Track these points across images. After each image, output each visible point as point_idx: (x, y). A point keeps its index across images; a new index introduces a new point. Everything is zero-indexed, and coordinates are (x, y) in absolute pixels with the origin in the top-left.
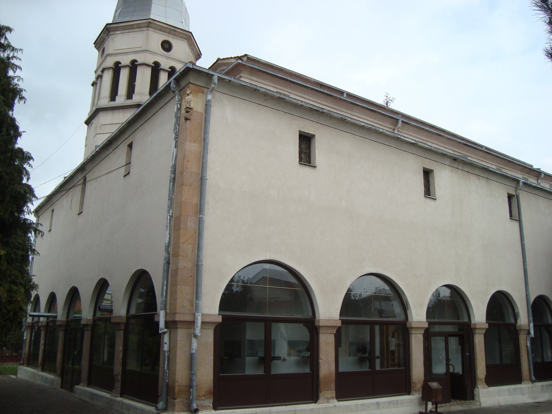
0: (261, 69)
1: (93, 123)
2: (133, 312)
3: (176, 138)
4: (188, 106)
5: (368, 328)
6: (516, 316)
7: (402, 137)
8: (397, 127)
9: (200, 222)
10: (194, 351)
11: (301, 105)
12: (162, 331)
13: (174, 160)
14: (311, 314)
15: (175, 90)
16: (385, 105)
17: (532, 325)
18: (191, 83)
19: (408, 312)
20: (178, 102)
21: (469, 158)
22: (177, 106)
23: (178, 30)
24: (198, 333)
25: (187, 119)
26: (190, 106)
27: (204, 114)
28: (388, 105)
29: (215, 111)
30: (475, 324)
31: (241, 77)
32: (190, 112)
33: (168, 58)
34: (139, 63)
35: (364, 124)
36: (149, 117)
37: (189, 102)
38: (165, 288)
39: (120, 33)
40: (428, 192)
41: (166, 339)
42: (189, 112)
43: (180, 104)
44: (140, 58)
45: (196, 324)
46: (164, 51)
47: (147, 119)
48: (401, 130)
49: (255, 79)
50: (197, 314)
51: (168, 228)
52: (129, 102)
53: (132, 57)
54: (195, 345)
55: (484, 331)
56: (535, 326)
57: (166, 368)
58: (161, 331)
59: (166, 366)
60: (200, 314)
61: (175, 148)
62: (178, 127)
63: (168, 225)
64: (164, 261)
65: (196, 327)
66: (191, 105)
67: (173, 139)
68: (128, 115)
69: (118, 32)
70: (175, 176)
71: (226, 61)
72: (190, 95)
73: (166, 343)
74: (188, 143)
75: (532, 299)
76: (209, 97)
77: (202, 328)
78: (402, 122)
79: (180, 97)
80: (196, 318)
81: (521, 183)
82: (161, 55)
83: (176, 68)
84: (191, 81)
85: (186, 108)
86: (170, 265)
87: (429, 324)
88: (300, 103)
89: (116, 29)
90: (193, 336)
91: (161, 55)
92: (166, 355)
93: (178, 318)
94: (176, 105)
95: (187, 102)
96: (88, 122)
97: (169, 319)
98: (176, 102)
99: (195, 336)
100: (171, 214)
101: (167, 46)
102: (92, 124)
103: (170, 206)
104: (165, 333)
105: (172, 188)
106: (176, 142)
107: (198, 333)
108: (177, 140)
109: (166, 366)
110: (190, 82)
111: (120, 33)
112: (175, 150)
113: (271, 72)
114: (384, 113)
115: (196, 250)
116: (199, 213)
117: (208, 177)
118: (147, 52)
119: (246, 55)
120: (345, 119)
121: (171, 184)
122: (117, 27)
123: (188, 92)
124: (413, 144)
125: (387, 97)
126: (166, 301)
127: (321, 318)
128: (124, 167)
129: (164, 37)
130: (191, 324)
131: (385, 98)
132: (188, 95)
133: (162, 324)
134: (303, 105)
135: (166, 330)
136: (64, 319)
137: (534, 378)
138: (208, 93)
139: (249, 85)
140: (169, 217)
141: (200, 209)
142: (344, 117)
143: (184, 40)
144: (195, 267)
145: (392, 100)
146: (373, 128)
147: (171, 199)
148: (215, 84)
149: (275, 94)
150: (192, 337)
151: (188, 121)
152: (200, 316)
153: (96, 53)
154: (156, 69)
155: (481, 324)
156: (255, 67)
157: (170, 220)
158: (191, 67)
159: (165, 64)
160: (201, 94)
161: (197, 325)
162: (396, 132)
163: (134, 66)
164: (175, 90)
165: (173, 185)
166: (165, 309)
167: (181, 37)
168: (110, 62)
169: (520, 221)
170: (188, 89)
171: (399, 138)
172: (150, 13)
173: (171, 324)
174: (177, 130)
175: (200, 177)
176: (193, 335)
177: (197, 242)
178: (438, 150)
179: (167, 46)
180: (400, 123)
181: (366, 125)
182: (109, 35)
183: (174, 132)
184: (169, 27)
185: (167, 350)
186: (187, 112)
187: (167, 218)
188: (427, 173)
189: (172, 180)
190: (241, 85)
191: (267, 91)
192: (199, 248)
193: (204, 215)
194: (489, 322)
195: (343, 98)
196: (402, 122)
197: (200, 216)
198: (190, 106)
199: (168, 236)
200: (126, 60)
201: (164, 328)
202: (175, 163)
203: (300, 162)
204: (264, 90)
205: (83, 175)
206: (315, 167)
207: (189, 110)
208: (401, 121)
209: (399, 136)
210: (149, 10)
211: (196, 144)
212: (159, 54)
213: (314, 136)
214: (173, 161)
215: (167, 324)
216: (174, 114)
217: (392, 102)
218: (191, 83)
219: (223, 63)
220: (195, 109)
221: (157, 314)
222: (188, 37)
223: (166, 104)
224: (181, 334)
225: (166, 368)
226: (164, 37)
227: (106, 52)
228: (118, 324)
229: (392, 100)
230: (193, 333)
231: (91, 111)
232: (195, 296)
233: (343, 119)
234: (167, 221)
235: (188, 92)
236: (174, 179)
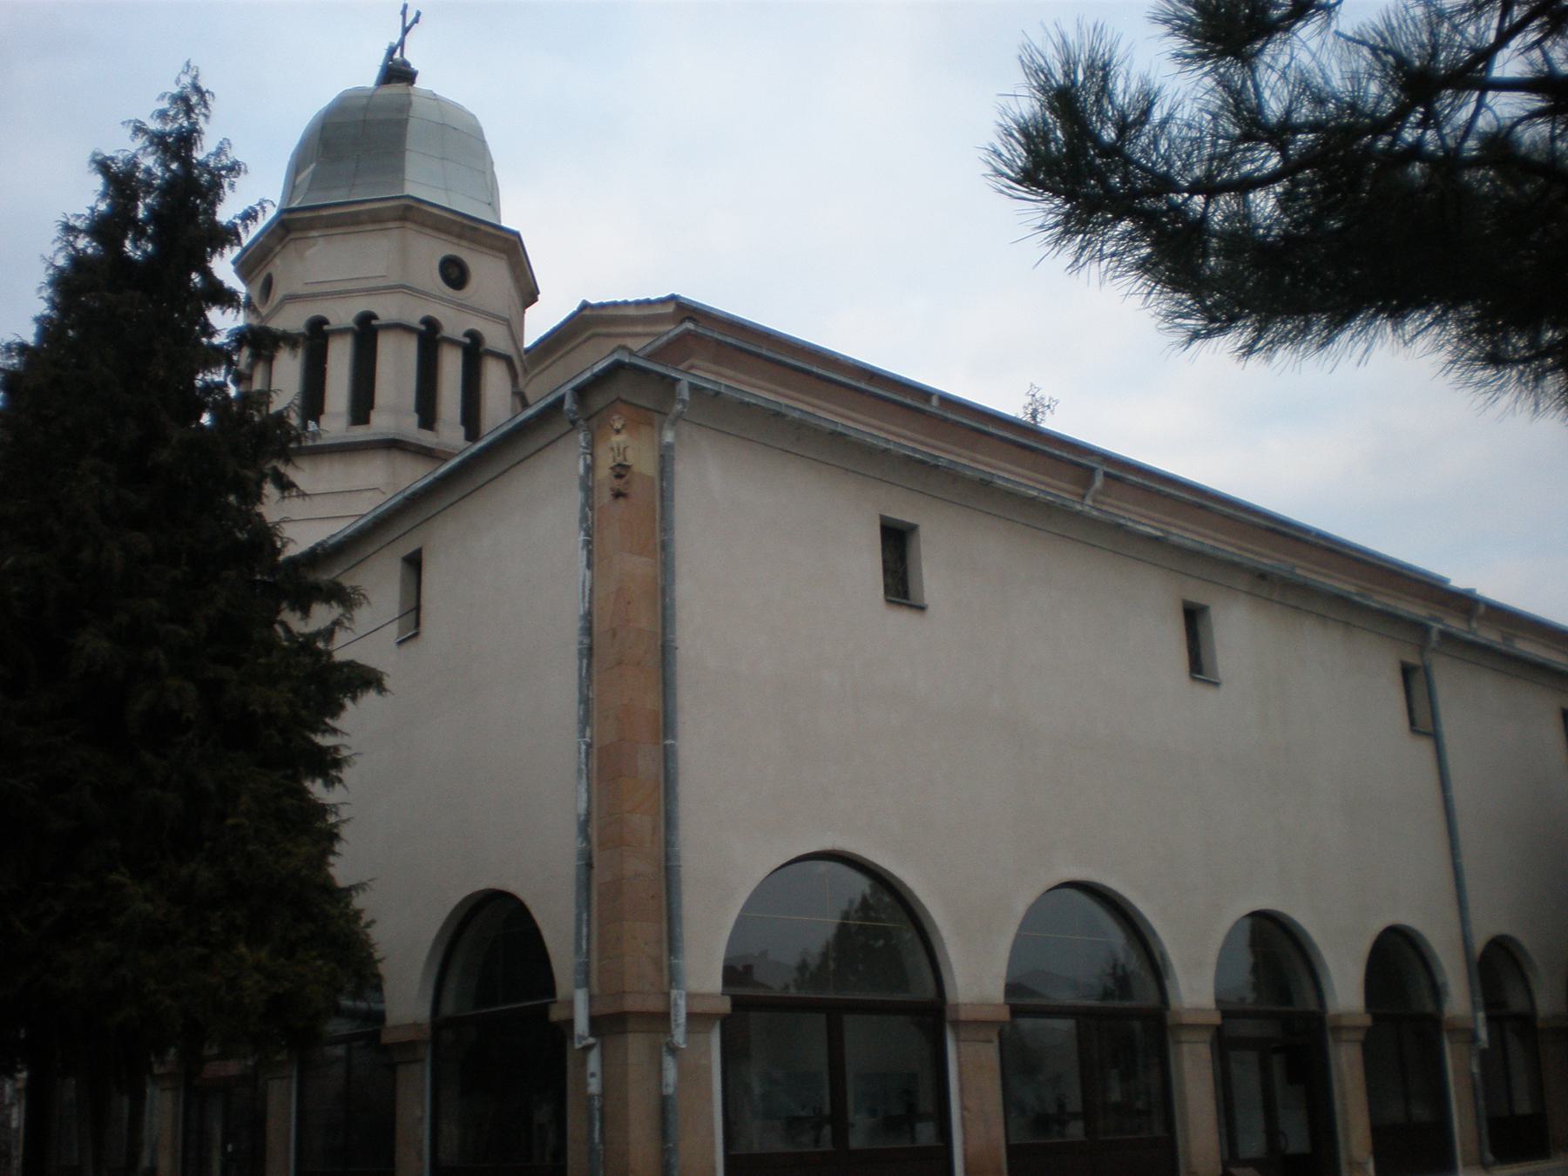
0: (746, 346)
3: (588, 544)
5: (821, 1020)
6: (1437, 992)
7: (1130, 524)
8: (1091, 492)
9: (668, 757)
10: (670, 1091)
11: (886, 450)
12: (584, 1043)
13: (587, 599)
14: (1065, 1025)
15: (577, 416)
16: (1028, 418)
17: (1481, 1015)
18: (625, 402)
19: (1168, 983)
20: (585, 448)
21: (1298, 571)
22: (585, 459)
23: (483, 227)
24: (681, 1041)
27: (657, 483)
28: (1038, 420)
29: (684, 471)
30: (1339, 1016)
31: (692, 367)
32: (626, 478)
33: (462, 307)
34: (383, 323)
35: (1035, 493)
36: (480, 482)
38: (585, 930)
39: (319, 236)
40: (1198, 665)
41: (594, 1062)
43: (591, 454)
44: (386, 309)
45: (673, 1018)
46: (448, 287)
47: (473, 488)
48: (1101, 498)
49: (729, 372)
50: (674, 992)
51: (584, 776)
52: (360, 433)
53: (360, 305)
54: (671, 1073)
55: (1360, 1036)
56: (1490, 1019)
57: (597, 1141)
58: (580, 1043)
59: (597, 1135)
60: (683, 993)
61: (587, 570)
62: (590, 514)
63: (583, 767)
64: (578, 859)
65: (673, 1026)
67: (580, 545)
68: (413, 475)
69: (314, 233)
70: (592, 641)
71: (610, 312)
73: (593, 1075)
75: (1479, 944)
76: (669, 437)
77: (689, 1032)
78: (1107, 475)
79: (589, 437)
80: (672, 1003)
81: (1434, 636)
82: (442, 299)
83: (481, 332)
84: (624, 397)
86: (595, 871)
88: (883, 445)
89: (310, 225)
90: (667, 1052)
91: (442, 299)
92: (597, 1104)
93: (632, 1004)
94: (582, 456)
97: (604, 1008)
98: (581, 450)
99: (673, 1050)
100: (588, 740)
101: (455, 274)
103: (585, 720)
104: (588, 1048)
105: (588, 671)
106: (590, 553)
107: (681, 1041)
108: (590, 547)
109: (597, 1135)
111: (319, 236)
112: (588, 573)
113: (770, 354)
114: (1057, 452)
115: (662, 829)
116: (661, 735)
117: (678, 643)
119: (673, 298)
120: (991, 482)
121: (585, 661)
122: (312, 219)
124: (1157, 539)
125: (1033, 396)
126: (587, 964)
127: (960, 1001)
128: (397, 621)
129: (444, 248)
130: (662, 1019)
131: (1029, 399)
133: (581, 1025)
134: (890, 449)
135: (591, 1040)
137: (1489, 1157)
138: (666, 425)
139: (763, 404)
140: (583, 747)
141: (666, 724)
142: (987, 478)
143: (503, 255)
144: (663, 873)
145: (1049, 406)
146: (1058, 501)
147: (585, 701)
148: (683, 401)
149: (823, 424)
150: (664, 1053)
151: (621, 501)
152: (683, 998)
154: (429, 338)
155: (1197, 1010)
156: (729, 340)
157: (588, 754)
158: (627, 360)
159: (454, 324)
161: (676, 1021)
162: (1088, 501)
163: (366, 332)
164: (577, 416)
165: (589, 665)
166: (586, 983)
167: (492, 248)
169: (1435, 736)
170: (616, 417)
171: (1121, 526)
172: (403, 180)
173: (608, 1024)
174: (590, 523)
175: (659, 643)
176: (664, 1049)
177: (662, 808)
178: (1220, 554)
179: (455, 274)
180: (1099, 481)
181: (1042, 495)
183: (581, 526)
184: (459, 219)
185: (597, 1093)
186: (619, 476)
187: (579, 748)
188: (1193, 617)
189: (585, 652)
190: (742, 403)
191: (805, 417)
192: (670, 821)
193: (674, 737)
195: (932, 410)
196: (1107, 475)
197: (669, 742)
199: (584, 796)
200: (342, 314)
201: (586, 1035)
202: (590, 608)
203: (890, 598)
204: (796, 415)
207: (621, 471)
208: (1102, 473)
209: (1122, 521)
210: (399, 170)
212: (435, 297)
213: (913, 528)
214: (584, 603)
215: (595, 1023)
216: (576, 482)
217: (1048, 412)
218: (625, 402)
219: (322, 217)
220: (635, 469)
221: (556, 1002)
222: (510, 247)
223: (539, 450)
224: (636, 1046)
225: (597, 1141)
226: (444, 248)
227: (279, 292)
228: (409, 1046)
229: (1049, 406)
230: (667, 1044)
232: (665, 945)
233: (985, 481)
234: (579, 758)
235: (618, 425)
236: (590, 649)
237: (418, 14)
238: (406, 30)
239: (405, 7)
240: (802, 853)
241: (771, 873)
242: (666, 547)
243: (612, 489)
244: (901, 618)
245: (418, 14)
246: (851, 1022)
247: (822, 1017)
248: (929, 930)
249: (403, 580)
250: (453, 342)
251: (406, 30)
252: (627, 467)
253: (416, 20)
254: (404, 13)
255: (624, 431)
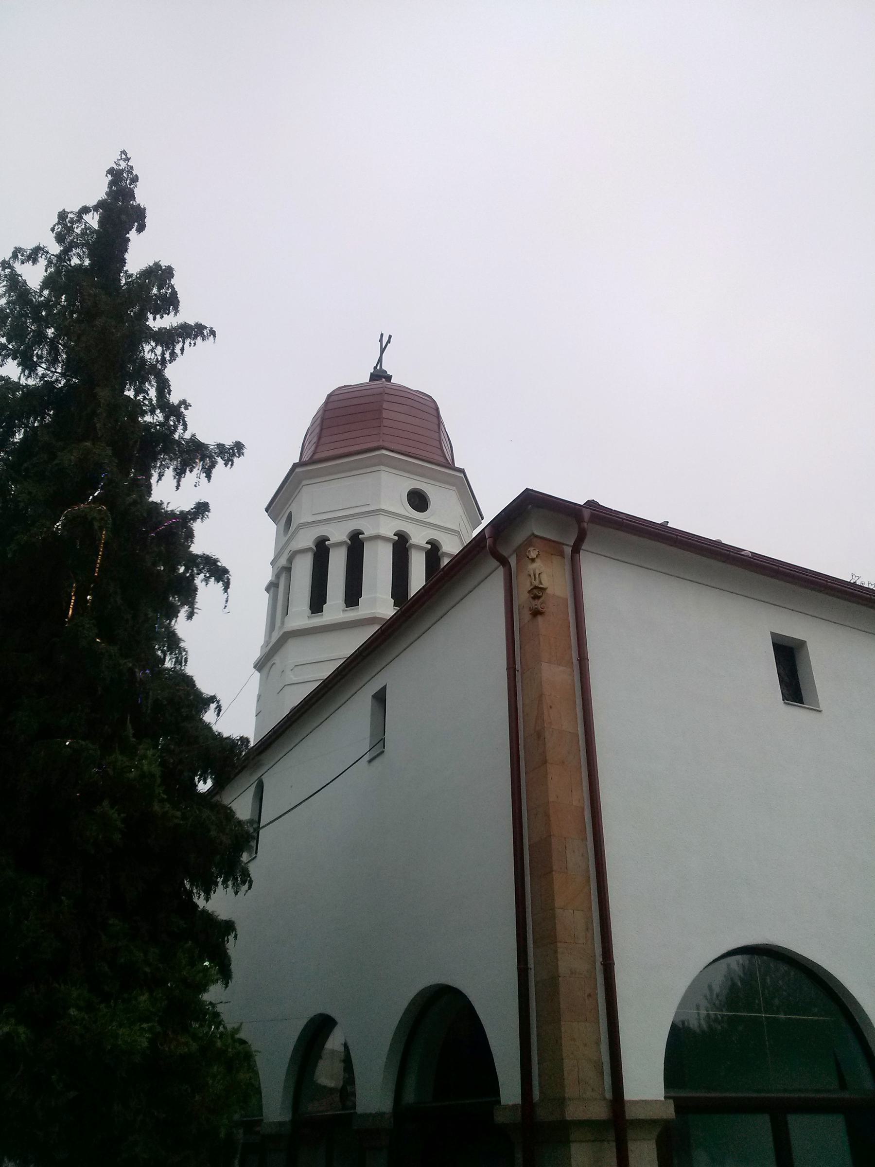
1: (274, 663)
2: (409, 1097)
4: (536, 583)
5: (762, 1123)
25: (536, 613)
26: (541, 584)
37: (537, 576)
42: (539, 597)
52: (353, 614)
66: (542, 581)
72: (536, 560)
74: (545, 666)
84: (536, 533)
85: (532, 589)
87: (678, 1109)
95: (532, 575)
96: (260, 666)
102: (273, 665)
110: (533, 534)
118: (381, 513)
123: (533, 554)
132: (533, 560)
136: (286, 1117)
151: (540, 619)
153: (269, 529)
159: (419, 537)
160: (560, 557)
168: (306, 540)
182: (302, 485)
194: (672, 1094)
198: (541, 584)
200: (338, 534)
205: (255, 777)
206: (820, 711)
207: (537, 592)
211: (561, 668)
231: (267, 643)
235: (533, 554)
237: (390, 337)
238: (382, 351)
239: (382, 335)
240: (739, 945)
241: (704, 969)
242: (583, 660)
243: (530, 609)
244: (795, 713)
245: (390, 337)
246: (797, 1123)
247: (766, 1118)
248: (862, 1026)
249: (373, 714)
250: (419, 548)
251: (382, 351)
252: (543, 590)
253: (389, 342)
254: (381, 340)
255: (538, 560)
